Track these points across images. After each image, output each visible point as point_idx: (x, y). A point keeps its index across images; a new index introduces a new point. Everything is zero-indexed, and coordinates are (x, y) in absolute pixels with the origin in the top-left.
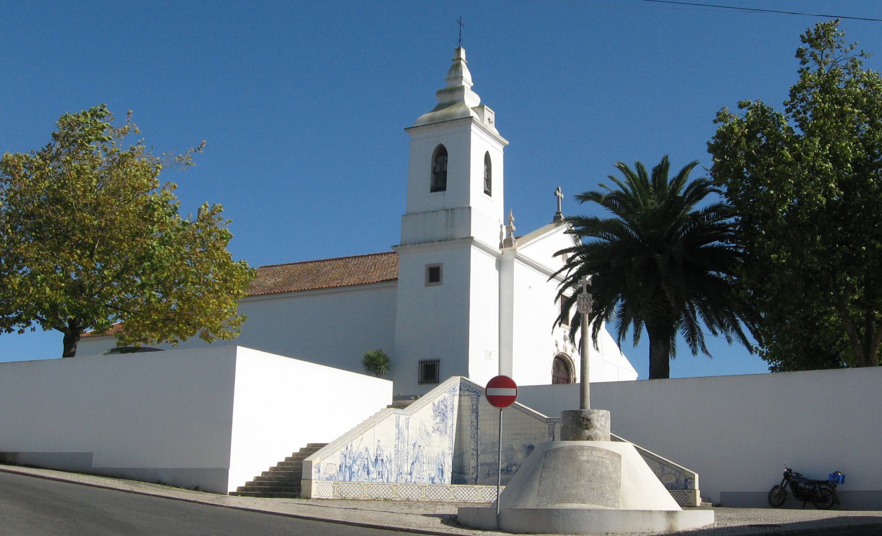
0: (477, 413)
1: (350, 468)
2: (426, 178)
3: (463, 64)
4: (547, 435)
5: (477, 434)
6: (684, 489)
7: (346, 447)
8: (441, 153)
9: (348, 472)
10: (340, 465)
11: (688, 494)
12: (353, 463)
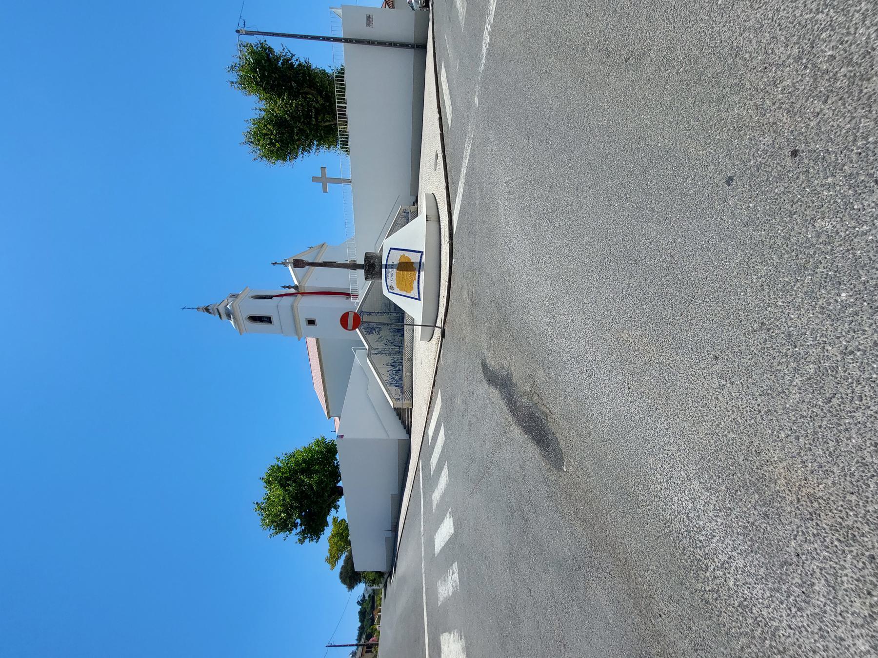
1: (397, 381)
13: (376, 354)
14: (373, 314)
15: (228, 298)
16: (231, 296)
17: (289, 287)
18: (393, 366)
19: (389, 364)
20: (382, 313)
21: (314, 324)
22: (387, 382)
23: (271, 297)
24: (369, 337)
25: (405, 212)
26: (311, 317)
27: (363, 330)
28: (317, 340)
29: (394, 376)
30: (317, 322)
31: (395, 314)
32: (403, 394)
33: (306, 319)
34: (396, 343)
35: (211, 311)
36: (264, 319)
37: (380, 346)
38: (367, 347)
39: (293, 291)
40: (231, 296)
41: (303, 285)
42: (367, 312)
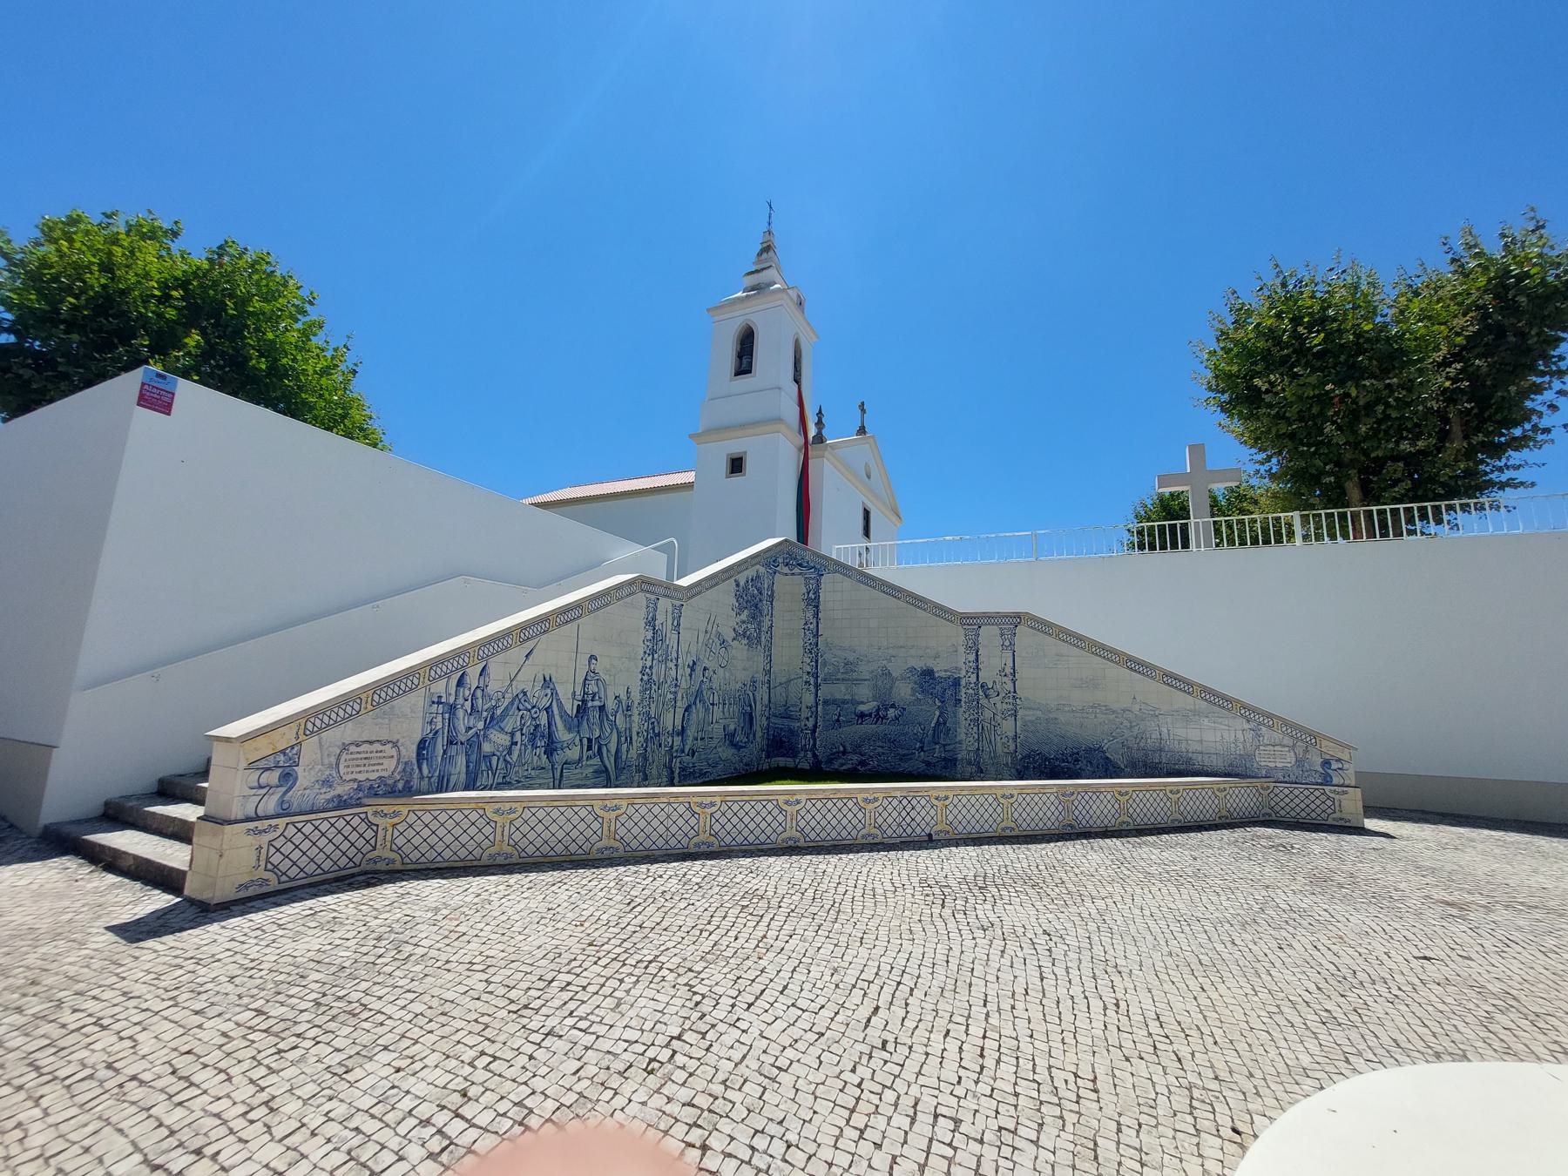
0: (817, 607)
1: (474, 744)
9: (461, 761)
12: (486, 728)
13: (651, 622)
14: (810, 615)
15: (795, 290)
16: (799, 296)
17: (819, 424)
18: (582, 710)
19: (592, 688)
20: (813, 649)
21: (733, 472)
22: (473, 679)
23: (797, 380)
24: (725, 597)
25: (1326, 763)
26: (749, 465)
27: (751, 573)
28: (688, 486)
29: (509, 724)
30: (737, 480)
31: (809, 699)
32: (341, 804)
33: (745, 453)
34: (698, 713)
35: (765, 255)
36: (744, 361)
37: (688, 642)
38: (685, 582)
39: (812, 432)
40: (799, 296)
41: (826, 453)
42: (817, 592)
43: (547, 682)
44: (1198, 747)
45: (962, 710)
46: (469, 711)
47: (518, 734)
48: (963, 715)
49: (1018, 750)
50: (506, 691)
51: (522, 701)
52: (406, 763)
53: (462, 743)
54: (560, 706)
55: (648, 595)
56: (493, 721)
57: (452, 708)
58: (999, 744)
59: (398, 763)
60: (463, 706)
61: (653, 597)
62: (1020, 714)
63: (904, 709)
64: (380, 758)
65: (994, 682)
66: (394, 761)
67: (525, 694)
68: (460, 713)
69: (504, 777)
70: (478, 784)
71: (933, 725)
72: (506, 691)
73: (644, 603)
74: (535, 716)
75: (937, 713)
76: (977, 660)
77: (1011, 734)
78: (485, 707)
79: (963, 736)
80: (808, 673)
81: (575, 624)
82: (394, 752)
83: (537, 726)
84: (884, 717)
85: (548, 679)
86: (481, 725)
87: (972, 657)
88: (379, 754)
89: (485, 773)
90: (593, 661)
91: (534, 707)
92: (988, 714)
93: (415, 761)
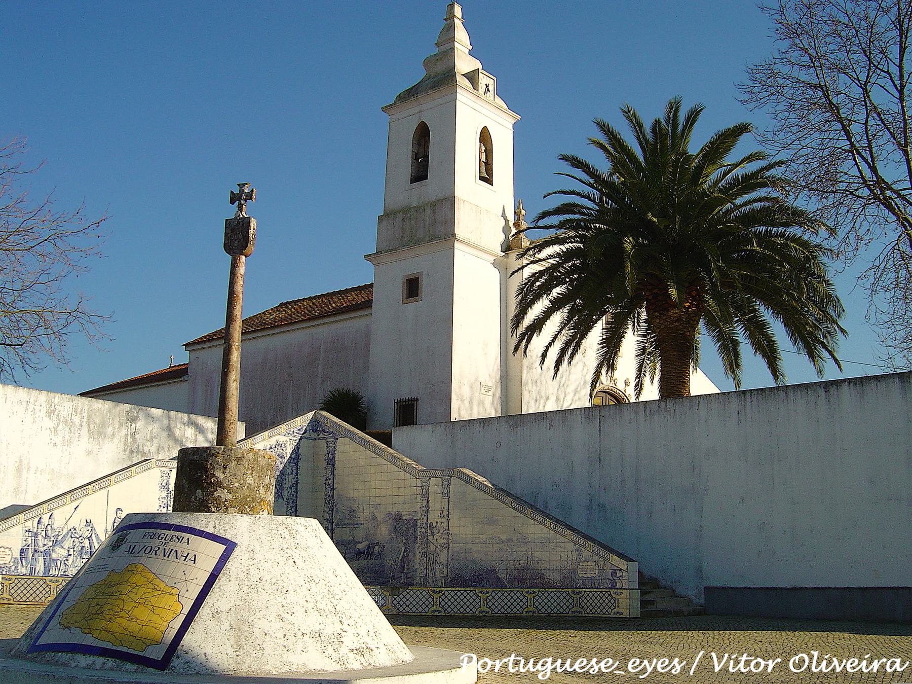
0: (333, 465)
1: (47, 553)
2: (406, 168)
3: (458, 23)
4: (419, 497)
5: (333, 498)
6: (611, 588)
7: (37, 520)
8: (423, 134)
9: (41, 560)
10: (22, 549)
11: (616, 597)
12: (53, 545)
25: (614, 572)
43: (88, 523)
44: (546, 566)
45: (418, 545)
46: (44, 537)
47: (72, 551)
48: (418, 549)
49: (449, 574)
50: (64, 527)
51: (73, 533)
52: (15, 558)
53: (41, 552)
54: (97, 535)
55: (161, 469)
56: (56, 543)
57: (36, 534)
58: (438, 571)
59: (12, 558)
60: (41, 534)
61: (167, 470)
62: (451, 545)
63: (384, 546)
64: (4, 555)
65: (437, 522)
66: (10, 556)
67: (75, 529)
68: (40, 537)
69: (64, 572)
70: (50, 573)
71: (400, 558)
72: (64, 527)
73: (159, 474)
74: (81, 541)
75: (404, 549)
76: (428, 505)
77: (445, 562)
78: (53, 535)
79: (417, 566)
80: (327, 520)
81: (106, 490)
82: (10, 553)
83: (82, 548)
84: (372, 554)
85: (89, 521)
86: (51, 544)
87: (425, 504)
88: (3, 553)
89: (54, 568)
90: (119, 511)
91: (81, 536)
92: (432, 548)
93: (19, 557)
